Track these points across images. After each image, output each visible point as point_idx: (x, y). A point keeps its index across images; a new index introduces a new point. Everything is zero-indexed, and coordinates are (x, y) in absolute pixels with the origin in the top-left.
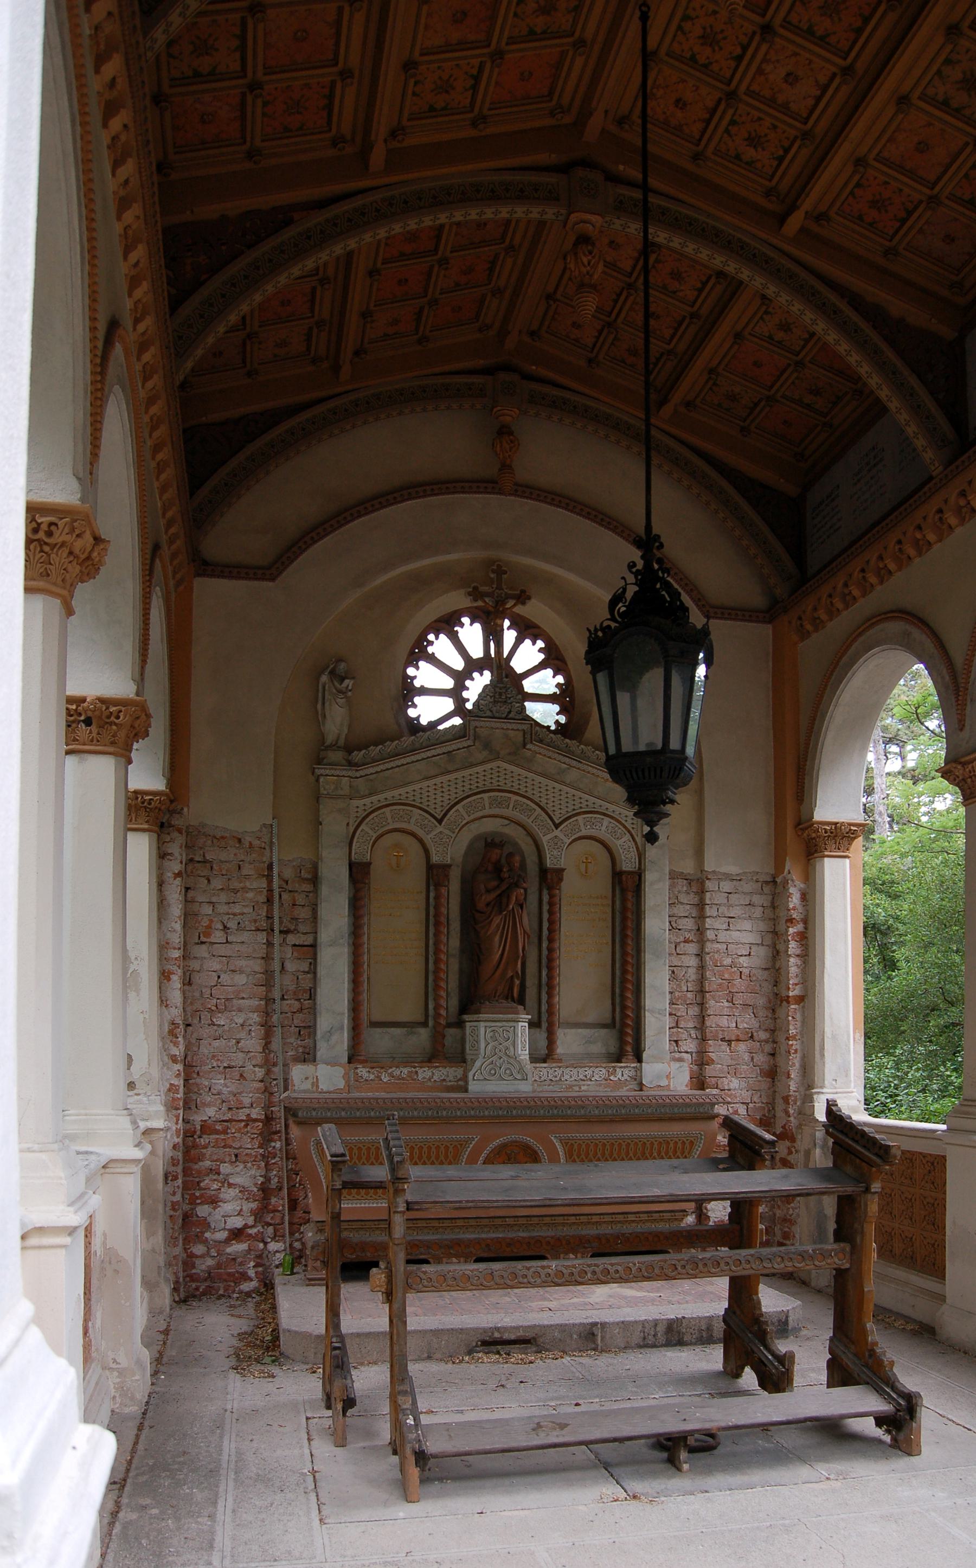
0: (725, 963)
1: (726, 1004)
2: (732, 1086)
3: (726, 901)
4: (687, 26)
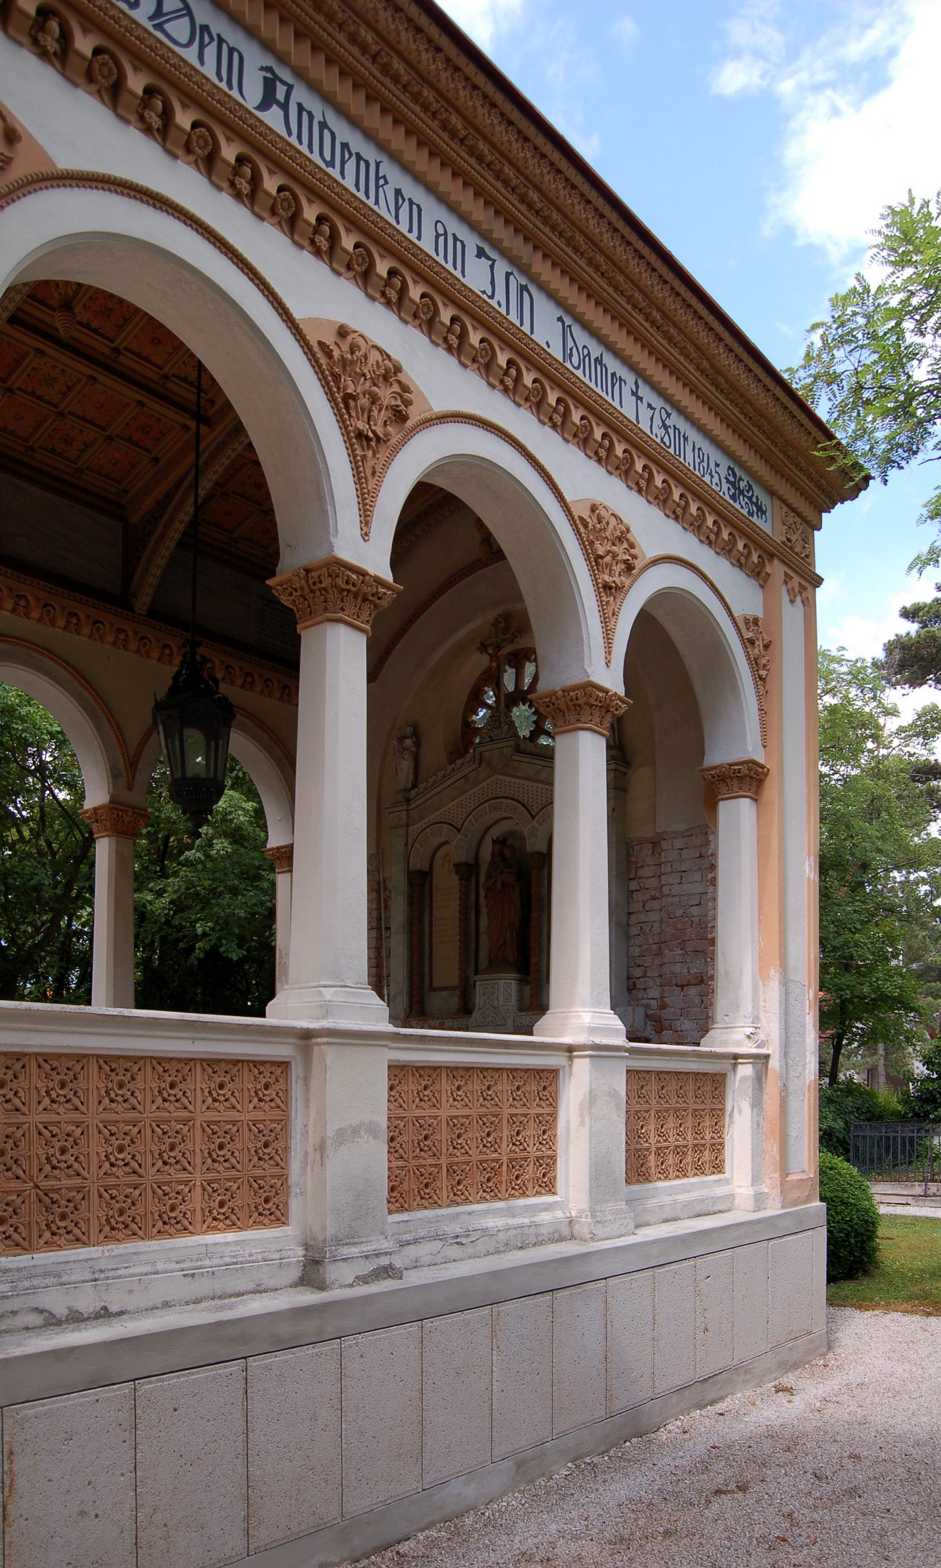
0: (677, 915)
1: (680, 952)
2: (684, 1028)
3: (678, 857)
4: (64, 389)
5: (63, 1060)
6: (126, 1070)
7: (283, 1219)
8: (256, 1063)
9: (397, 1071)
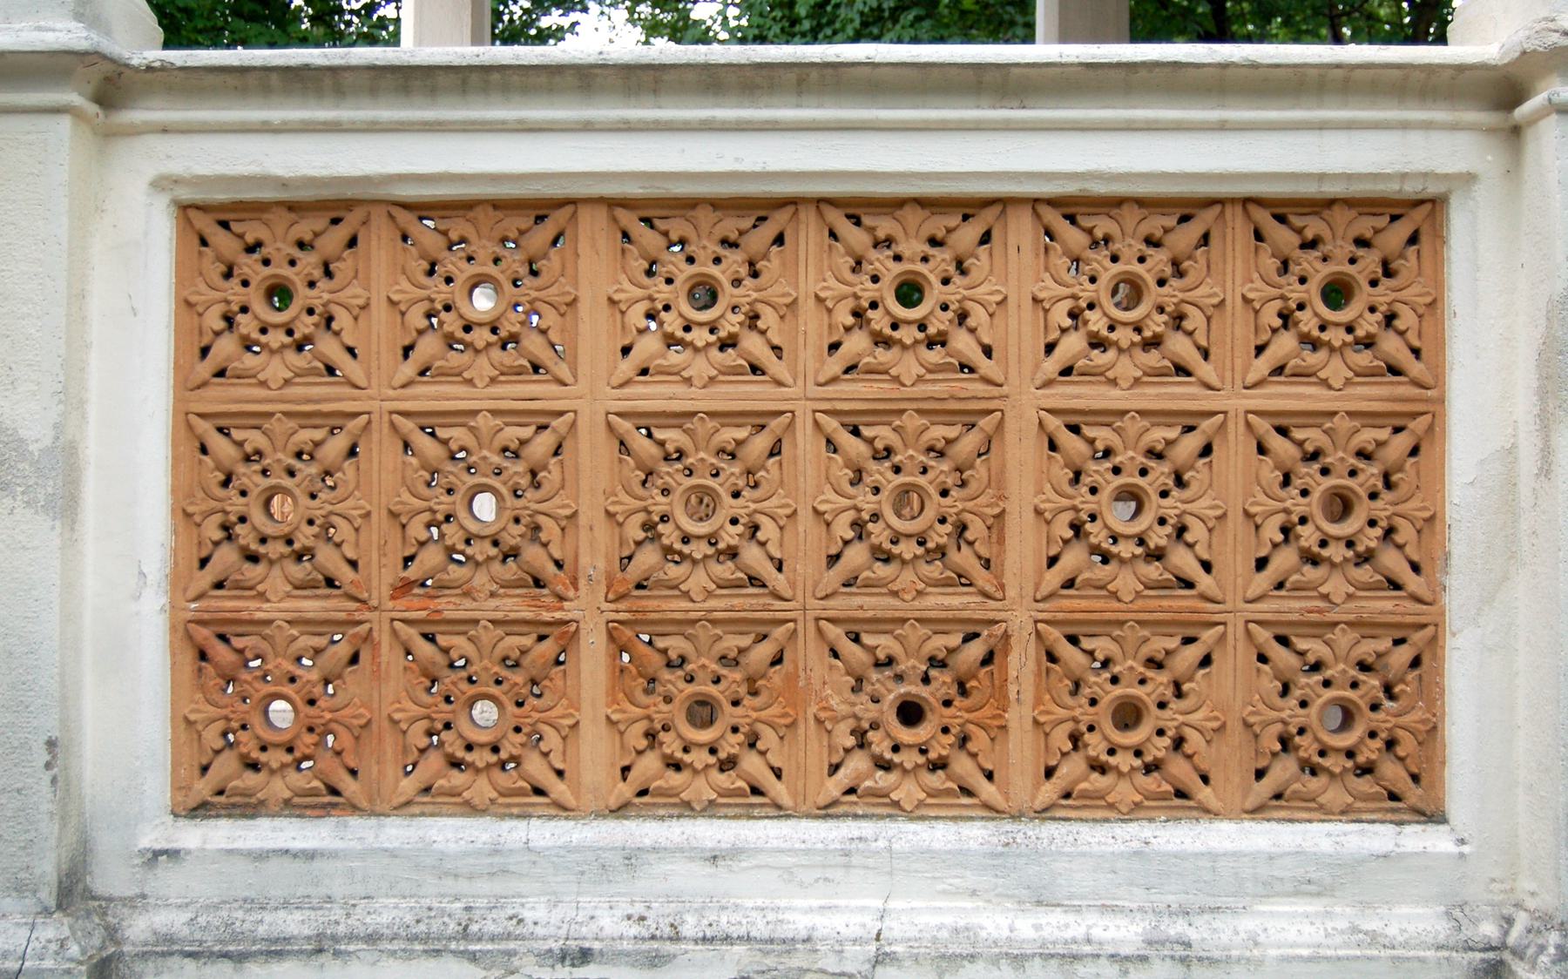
5: (704, 216)
6: (1362, 242)
7: (1413, 794)
8: (856, 209)
9: (216, 224)
